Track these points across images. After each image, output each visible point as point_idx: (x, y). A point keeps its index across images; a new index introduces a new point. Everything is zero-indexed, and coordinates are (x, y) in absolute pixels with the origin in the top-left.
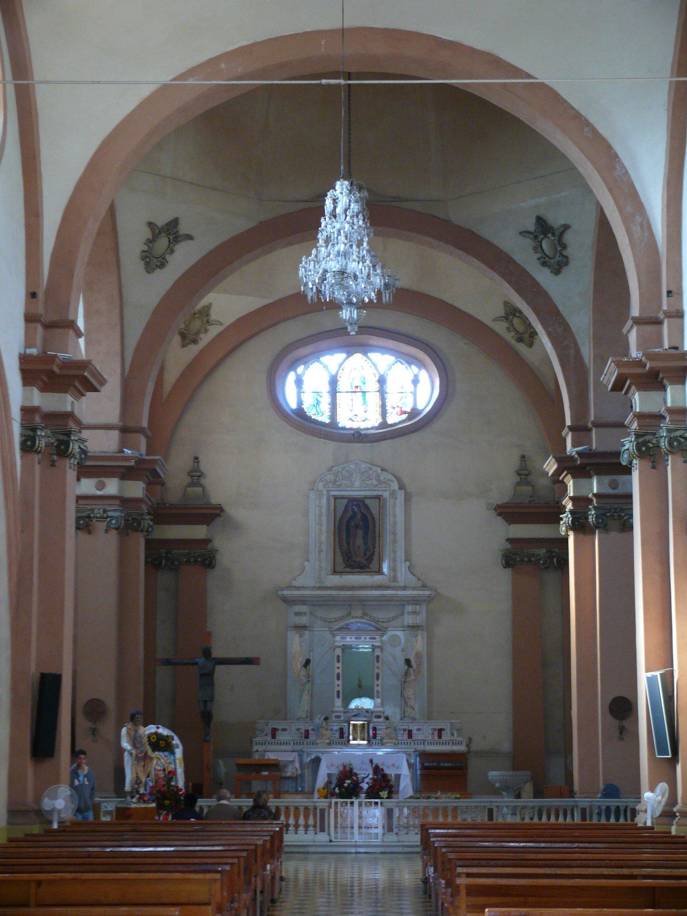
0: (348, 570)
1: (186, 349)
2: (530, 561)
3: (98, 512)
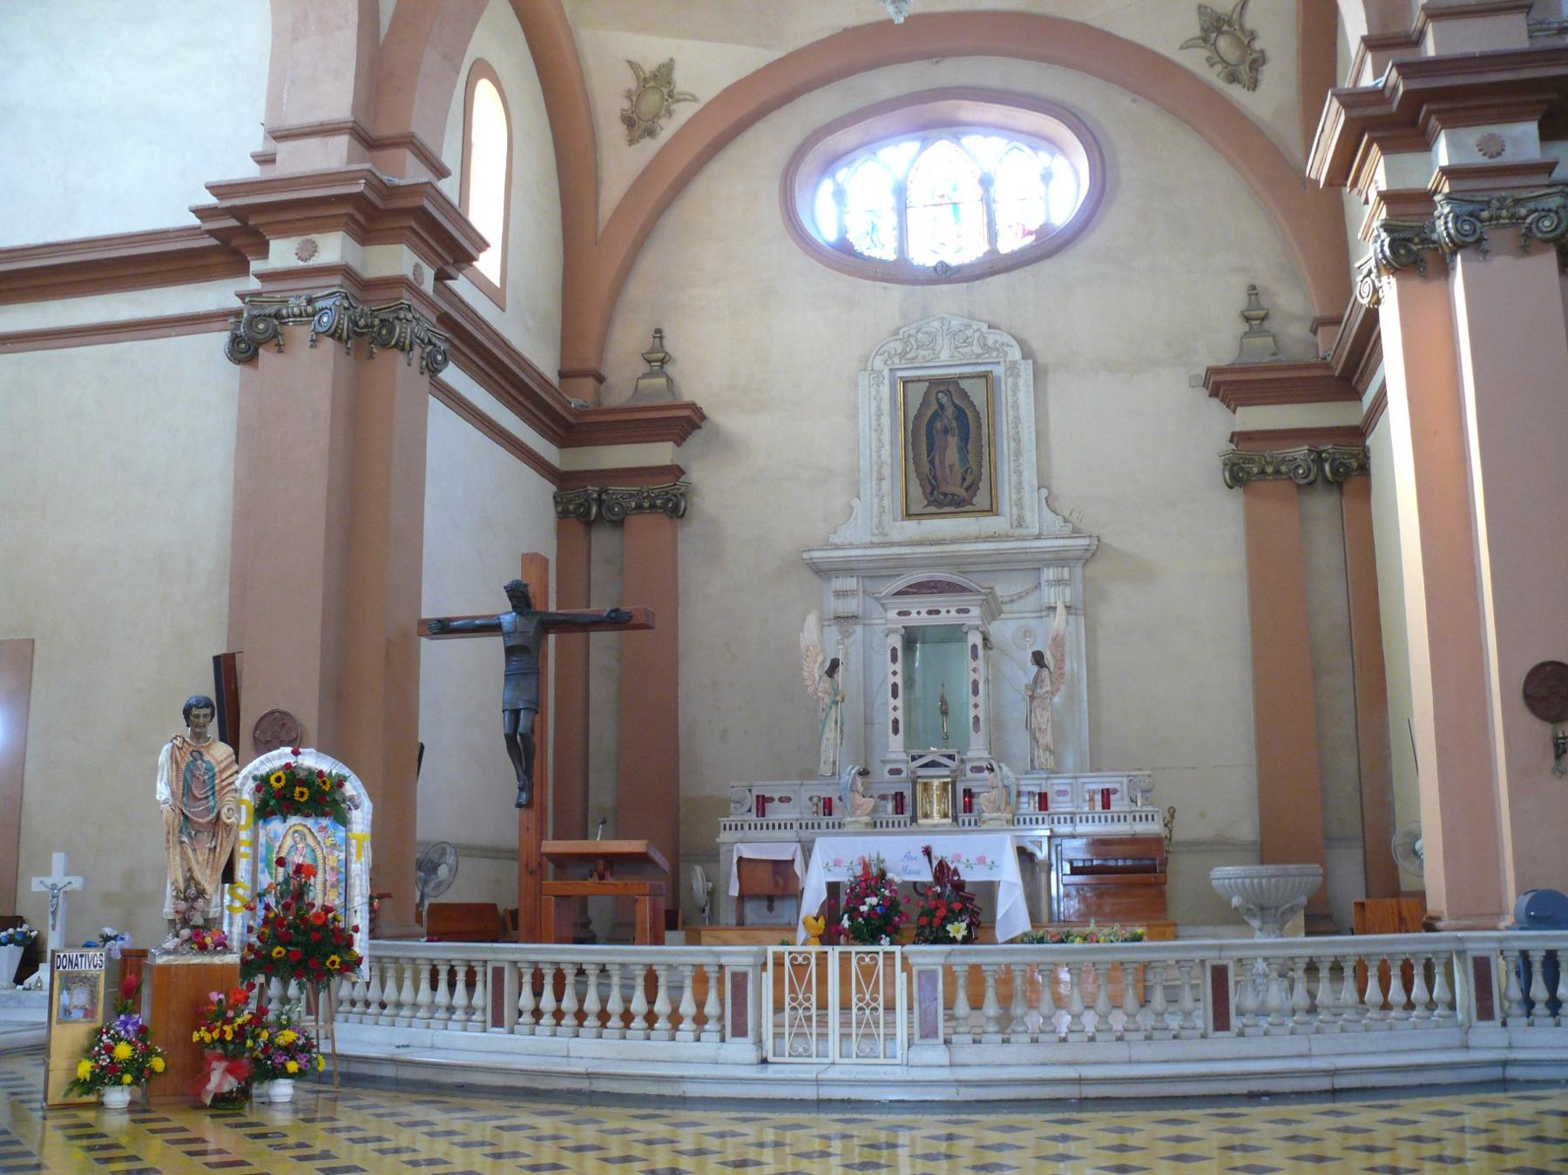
0: (932, 509)
1: (637, 146)
2: (1277, 472)
3: (296, 304)
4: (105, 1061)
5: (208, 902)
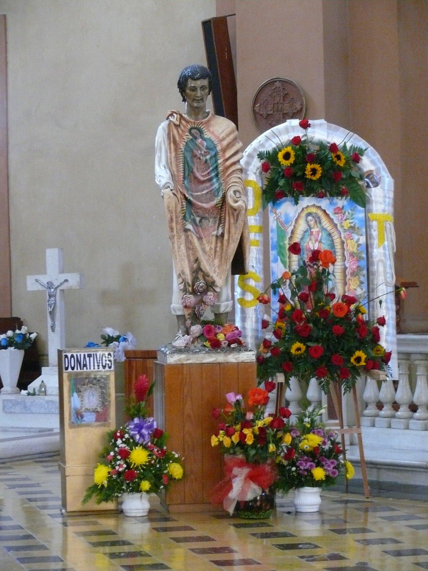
4: (121, 466)
5: (218, 295)
